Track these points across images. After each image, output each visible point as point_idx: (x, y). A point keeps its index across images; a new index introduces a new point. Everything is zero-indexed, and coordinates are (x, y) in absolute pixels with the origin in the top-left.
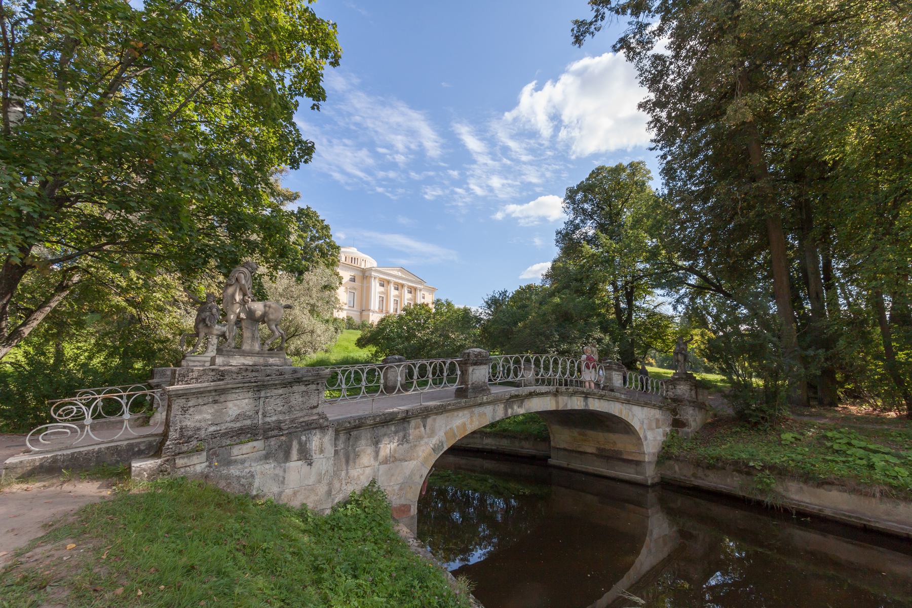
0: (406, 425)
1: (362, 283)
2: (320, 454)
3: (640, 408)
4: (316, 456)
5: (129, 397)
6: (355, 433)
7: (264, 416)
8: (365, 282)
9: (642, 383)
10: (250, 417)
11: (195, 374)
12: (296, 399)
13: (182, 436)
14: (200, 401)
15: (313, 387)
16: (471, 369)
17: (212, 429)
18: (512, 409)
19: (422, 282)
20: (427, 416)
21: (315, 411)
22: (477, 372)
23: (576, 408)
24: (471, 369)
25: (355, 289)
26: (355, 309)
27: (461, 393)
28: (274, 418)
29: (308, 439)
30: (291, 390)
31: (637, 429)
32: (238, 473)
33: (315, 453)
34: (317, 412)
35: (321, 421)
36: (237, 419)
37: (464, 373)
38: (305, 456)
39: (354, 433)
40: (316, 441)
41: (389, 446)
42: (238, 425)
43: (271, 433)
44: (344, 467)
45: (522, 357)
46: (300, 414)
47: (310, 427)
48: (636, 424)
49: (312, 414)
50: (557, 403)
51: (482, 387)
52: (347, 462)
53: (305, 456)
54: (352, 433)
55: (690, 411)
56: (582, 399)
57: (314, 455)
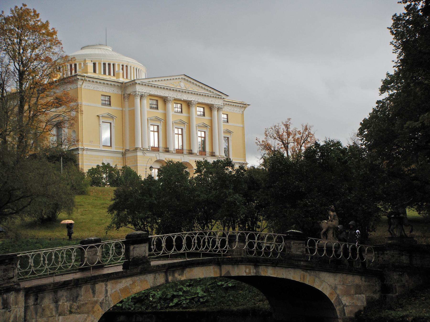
0: (78, 289)
1: (122, 106)
2: (16, 305)
3: (331, 274)
5: (30, 268)
6: (41, 295)
8: (127, 104)
9: (115, 264)
15: (11, 266)
16: (132, 247)
18: (173, 276)
19: (220, 94)
20: (94, 284)
22: (138, 249)
23: (244, 275)
24: (132, 247)
25: (112, 117)
26: (113, 149)
31: (327, 294)
33: (13, 305)
34: (13, 281)
35: (16, 286)
37: (127, 251)
39: (40, 295)
40: (12, 297)
41: (66, 303)
44: (34, 316)
49: (10, 282)
51: (142, 260)
52: (36, 313)
54: (39, 295)
55: (396, 276)
57: (12, 306)
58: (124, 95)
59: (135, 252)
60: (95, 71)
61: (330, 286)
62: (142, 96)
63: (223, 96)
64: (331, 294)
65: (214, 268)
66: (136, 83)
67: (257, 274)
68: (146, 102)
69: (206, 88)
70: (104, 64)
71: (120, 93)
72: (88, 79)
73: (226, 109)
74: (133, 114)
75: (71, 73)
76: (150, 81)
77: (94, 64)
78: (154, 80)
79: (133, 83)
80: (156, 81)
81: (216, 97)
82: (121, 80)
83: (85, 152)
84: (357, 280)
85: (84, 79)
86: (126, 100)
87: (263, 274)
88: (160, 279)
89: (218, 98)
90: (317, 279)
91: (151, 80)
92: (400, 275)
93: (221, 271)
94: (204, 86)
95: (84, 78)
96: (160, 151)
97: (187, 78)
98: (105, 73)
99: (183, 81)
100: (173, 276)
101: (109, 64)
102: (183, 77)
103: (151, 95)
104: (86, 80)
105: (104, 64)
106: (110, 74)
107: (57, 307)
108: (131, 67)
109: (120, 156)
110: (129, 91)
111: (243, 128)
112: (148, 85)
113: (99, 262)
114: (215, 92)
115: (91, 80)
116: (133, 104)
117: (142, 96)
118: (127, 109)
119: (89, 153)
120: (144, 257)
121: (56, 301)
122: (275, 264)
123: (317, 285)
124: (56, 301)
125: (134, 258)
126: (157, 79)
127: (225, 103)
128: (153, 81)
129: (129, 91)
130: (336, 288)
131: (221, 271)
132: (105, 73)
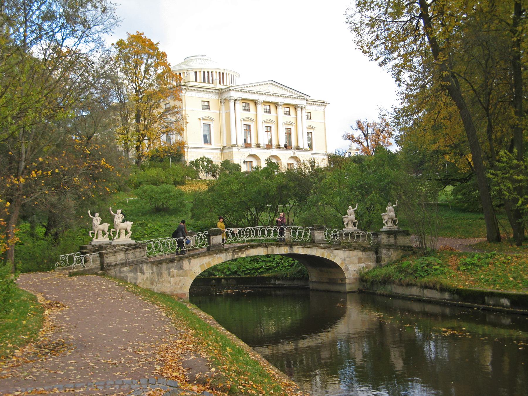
0: (181, 262)
3: (342, 251)
4: (145, 272)
7: (128, 259)
10: (124, 260)
11: (108, 247)
12: (137, 254)
13: (107, 265)
14: (110, 255)
15: (142, 249)
16: (211, 237)
17: (115, 263)
18: (238, 255)
19: (302, 96)
20: (190, 259)
21: (144, 257)
25: (211, 120)
27: (208, 249)
28: (131, 260)
29: (142, 266)
30: (135, 251)
32: (123, 276)
36: (121, 260)
38: (142, 272)
42: (121, 262)
43: (131, 264)
45: (184, 238)
46: (139, 258)
47: (142, 262)
48: (338, 261)
50: (273, 251)
51: (218, 245)
52: (158, 276)
53: (142, 272)
56: (288, 248)
58: (221, 100)
59: (213, 241)
60: (196, 81)
61: (341, 259)
62: (235, 101)
63: (306, 97)
64: (342, 264)
65: (263, 250)
66: (230, 90)
67: (292, 253)
68: (240, 106)
69: (291, 90)
70: (204, 72)
71: (217, 98)
72: (190, 88)
73: (309, 108)
74: (228, 115)
75: (177, 83)
76: (242, 88)
77: (196, 73)
78: (246, 86)
79: (228, 89)
80: (247, 87)
81: (300, 98)
82: (219, 86)
83: (189, 150)
84: (360, 254)
85: (188, 88)
86: (223, 104)
87: (296, 252)
88: (229, 256)
89: (302, 99)
90: (332, 254)
91: (243, 86)
92: (387, 250)
93: (268, 251)
94: (289, 89)
95: (187, 88)
96: (253, 146)
97: (274, 83)
98: (204, 82)
99: (271, 85)
100: (238, 255)
101: (208, 72)
102: (271, 82)
103: (243, 99)
104: (189, 89)
105: (219, 73)
106: (209, 82)
107: (169, 274)
108: (226, 74)
109: (219, 152)
110: (225, 96)
111: (325, 123)
112: (241, 91)
113: (192, 247)
114: (299, 94)
115: (193, 88)
116: (228, 108)
117: (235, 101)
118: (223, 111)
119: (193, 150)
120: (220, 243)
121: (169, 269)
122: (303, 245)
123: (331, 258)
124: (169, 269)
125: (213, 244)
126: (248, 86)
127: (308, 102)
128: (244, 87)
129: (225, 96)
130: (344, 260)
131: (268, 251)
132: (204, 82)
